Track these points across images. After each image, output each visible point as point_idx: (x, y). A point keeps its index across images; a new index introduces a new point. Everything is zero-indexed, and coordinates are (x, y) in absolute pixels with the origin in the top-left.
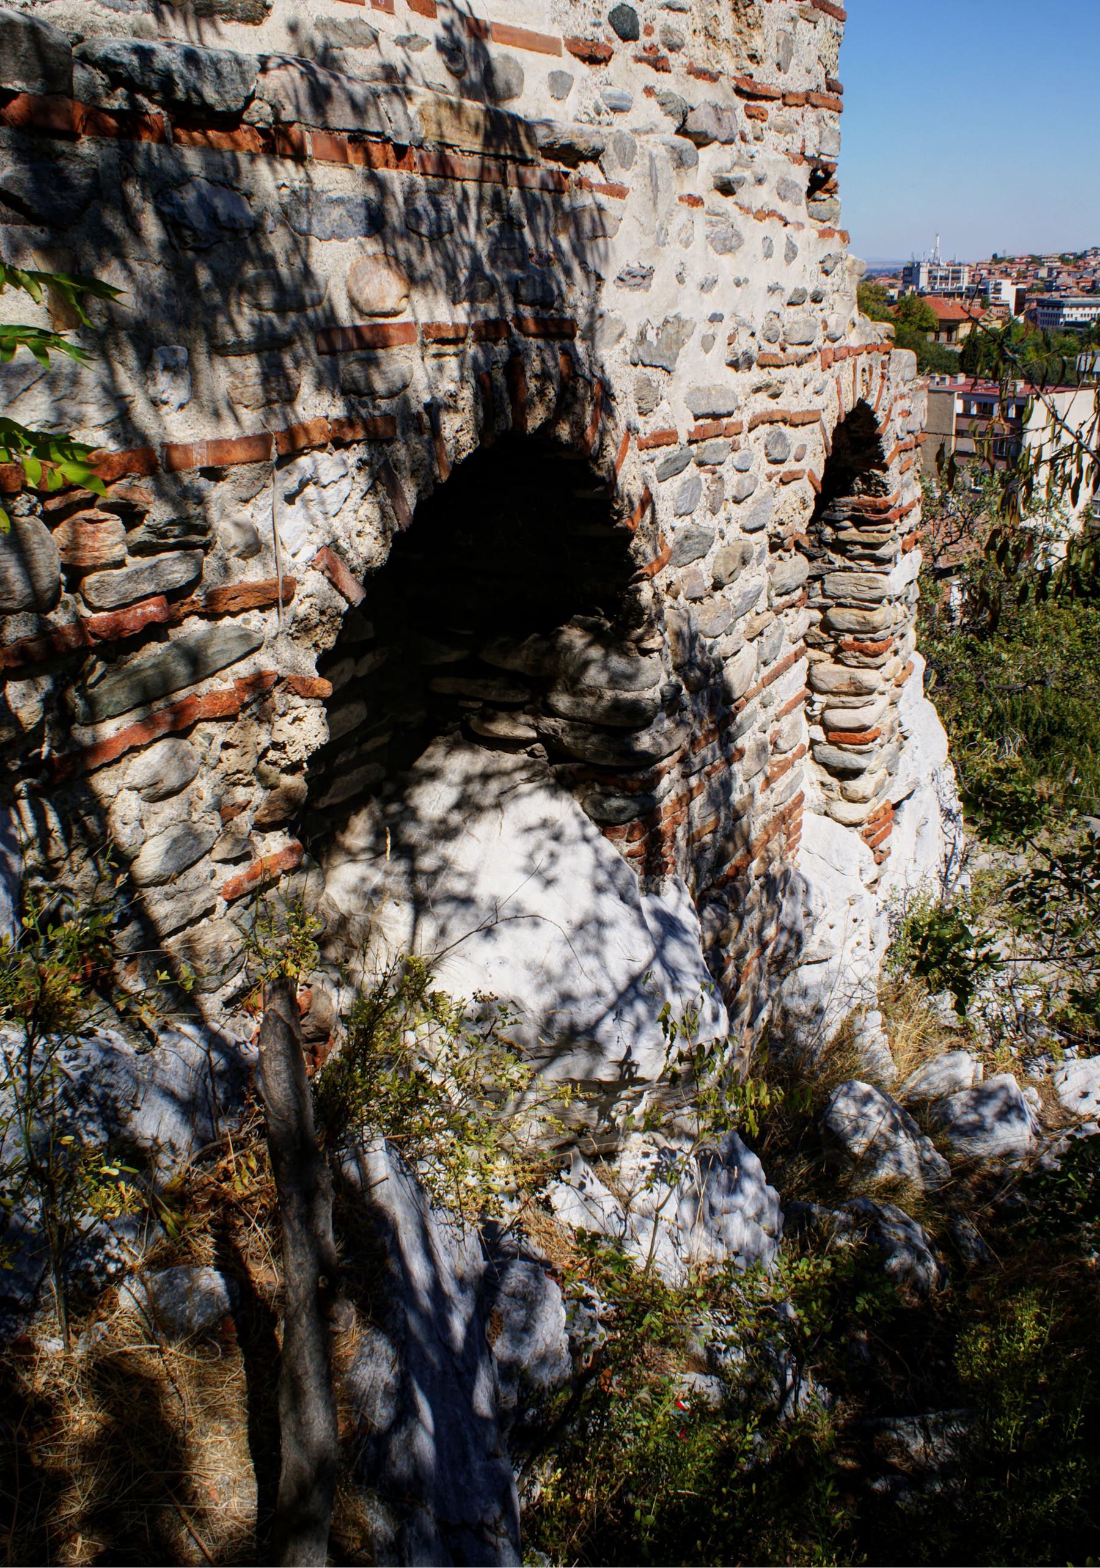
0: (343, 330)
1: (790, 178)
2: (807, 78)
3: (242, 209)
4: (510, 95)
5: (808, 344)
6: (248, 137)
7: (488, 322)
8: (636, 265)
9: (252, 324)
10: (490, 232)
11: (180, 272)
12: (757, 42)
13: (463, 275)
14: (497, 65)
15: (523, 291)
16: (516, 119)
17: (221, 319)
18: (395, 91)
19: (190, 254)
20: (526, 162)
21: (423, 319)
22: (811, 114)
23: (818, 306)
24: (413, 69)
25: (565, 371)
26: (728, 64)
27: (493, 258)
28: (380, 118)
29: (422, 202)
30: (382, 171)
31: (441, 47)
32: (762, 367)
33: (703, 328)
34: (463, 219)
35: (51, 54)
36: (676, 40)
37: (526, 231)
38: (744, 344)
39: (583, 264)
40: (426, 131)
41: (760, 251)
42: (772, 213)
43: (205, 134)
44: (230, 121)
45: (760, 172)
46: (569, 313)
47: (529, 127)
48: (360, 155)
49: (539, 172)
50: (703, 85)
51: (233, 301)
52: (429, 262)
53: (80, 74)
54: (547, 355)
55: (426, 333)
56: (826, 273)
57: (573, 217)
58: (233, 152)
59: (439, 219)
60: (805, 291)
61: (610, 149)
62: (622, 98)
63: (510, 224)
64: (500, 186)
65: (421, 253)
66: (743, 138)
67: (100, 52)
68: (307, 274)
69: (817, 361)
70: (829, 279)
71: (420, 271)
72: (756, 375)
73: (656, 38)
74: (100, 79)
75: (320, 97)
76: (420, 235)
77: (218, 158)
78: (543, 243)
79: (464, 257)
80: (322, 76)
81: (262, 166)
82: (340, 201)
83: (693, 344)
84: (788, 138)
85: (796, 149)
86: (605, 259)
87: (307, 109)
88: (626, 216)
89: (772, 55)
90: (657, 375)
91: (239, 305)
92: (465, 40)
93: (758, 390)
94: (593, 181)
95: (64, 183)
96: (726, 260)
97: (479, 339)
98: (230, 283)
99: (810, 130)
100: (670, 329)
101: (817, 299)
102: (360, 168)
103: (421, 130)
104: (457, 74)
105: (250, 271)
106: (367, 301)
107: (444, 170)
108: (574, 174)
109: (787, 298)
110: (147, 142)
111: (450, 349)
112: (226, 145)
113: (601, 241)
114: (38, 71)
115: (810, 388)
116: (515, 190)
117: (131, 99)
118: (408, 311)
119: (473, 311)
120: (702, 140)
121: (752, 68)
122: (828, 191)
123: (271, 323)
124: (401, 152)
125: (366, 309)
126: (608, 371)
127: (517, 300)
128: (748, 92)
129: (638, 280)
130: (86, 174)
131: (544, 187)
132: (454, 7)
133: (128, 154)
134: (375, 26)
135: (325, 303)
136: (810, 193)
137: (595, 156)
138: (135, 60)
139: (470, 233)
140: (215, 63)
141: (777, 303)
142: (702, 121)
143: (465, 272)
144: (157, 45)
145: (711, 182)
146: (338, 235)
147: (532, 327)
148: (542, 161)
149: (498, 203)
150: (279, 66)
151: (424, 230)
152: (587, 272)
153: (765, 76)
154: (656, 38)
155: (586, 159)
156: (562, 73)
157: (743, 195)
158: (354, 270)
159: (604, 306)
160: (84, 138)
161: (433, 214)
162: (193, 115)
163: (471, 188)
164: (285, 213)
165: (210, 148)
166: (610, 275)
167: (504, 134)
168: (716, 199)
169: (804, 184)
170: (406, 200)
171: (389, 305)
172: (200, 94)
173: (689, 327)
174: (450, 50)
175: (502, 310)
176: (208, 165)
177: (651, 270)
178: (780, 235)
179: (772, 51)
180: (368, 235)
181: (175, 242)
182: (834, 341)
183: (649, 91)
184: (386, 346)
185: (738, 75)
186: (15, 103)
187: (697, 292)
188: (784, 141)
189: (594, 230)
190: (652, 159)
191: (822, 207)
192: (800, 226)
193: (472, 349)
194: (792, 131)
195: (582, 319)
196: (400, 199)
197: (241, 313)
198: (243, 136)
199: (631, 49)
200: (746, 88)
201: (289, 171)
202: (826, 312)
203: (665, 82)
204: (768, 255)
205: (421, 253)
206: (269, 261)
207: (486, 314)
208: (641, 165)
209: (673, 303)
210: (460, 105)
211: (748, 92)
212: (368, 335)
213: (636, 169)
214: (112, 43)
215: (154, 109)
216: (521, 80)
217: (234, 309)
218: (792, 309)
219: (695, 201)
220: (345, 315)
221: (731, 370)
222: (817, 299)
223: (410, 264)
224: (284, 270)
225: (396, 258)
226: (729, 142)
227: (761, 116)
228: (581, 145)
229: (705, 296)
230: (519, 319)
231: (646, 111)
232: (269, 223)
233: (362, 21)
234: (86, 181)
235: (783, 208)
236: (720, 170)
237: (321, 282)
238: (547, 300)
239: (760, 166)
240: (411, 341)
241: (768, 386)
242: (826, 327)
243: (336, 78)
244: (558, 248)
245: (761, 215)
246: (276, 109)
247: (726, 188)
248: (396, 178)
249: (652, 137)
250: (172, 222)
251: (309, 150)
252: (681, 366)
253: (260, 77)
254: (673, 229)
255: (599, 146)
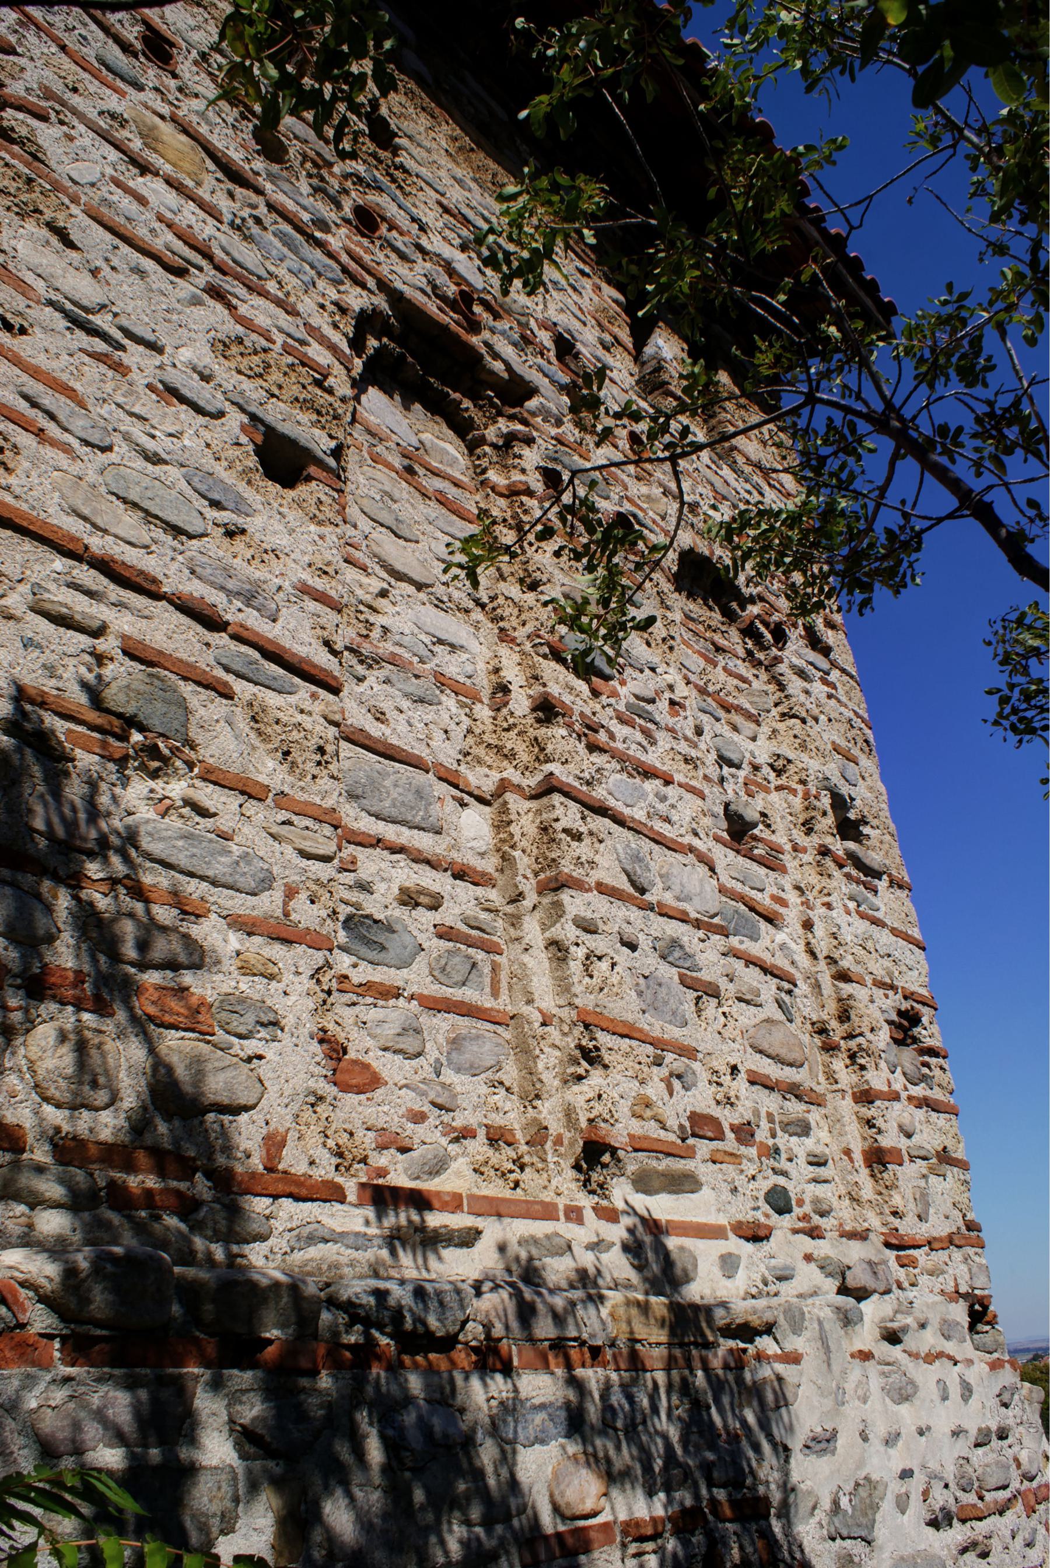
0: (546, 1538)
1: (950, 1317)
2: (947, 1222)
3: (456, 1425)
4: (688, 1279)
5: (1005, 1487)
6: (463, 1355)
7: (684, 1512)
8: (819, 1429)
9: (461, 1542)
10: (679, 1418)
11: (396, 1489)
12: (897, 1200)
13: (658, 1464)
14: (675, 1255)
15: (715, 1475)
16: (695, 1308)
17: (433, 1539)
18: (590, 1297)
19: (408, 1474)
20: (708, 1345)
21: (622, 1516)
22: (957, 1255)
23: (1006, 1443)
24: (603, 1270)
25: (765, 1557)
26: (874, 1221)
27: (685, 1440)
28: (577, 1325)
29: (617, 1398)
30: (579, 1372)
31: (626, 1248)
32: (964, 1521)
33: (896, 1487)
34: (655, 1410)
35: (305, 1305)
36: (825, 1207)
37: (713, 1410)
38: (940, 1498)
39: (770, 1436)
40: (618, 1331)
41: (935, 1393)
42: (940, 1355)
43: (426, 1357)
44: (447, 1343)
45: (922, 1317)
46: (761, 1489)
47: (708, 1310)
48: (561, 1359)
49: (721, 1352)
50: (855, 1245)
51: (444, 1519)
52: (625, 1457)
53: (326, 1316)
54: (746, 1543)
55: (625, 1533)
56: (1006, 1405)
57: (756, 1391)
58: (450, 1372)
59: (633, 1410)
60: (988, 1429)
61: (781, 1320)
62: (786, 1268)
63: (697, 1406)
64: (687, 1372)
65: (618, 1448)
66: (900, 1287)
67: (345, 1295)
68: (513, 1484)
69: (1019, 1506)
70: (1010, 1412)
71: (618, 1465)
72: (958, 1534)
73: (807, 1208)
74: (342, 1318)
75: (526, 1312)
76: (616, 1429)
77: (436, 1379)
78: (730, 1420)
79: (658, 1447)
80: (528, 1294)
81: (475, 1383)
82: (542, 1407)
83: (887, 1506)
84: (941, 1279)
85: (950, 1288)
86: (790, 1429)
87: (514, 1324)
88: (804, 1379)
89: (911, 1210)
90: (856, 1548)
91: (450, 1523)
92: (648, 1239)
93: (964, 1550)
94: (770, 1352)
95: (301, 1415)
96: (904, 1409)
97: (677, 1532)
98: (445, 1503)
99: (958, 1268)
100: (863, 1493)
101: (1002, 1435)
102: (560, 1372)
103: (612, 1330)
104: (639, 1268)
105: (462, 1487)
106: (568, 1504)
107: (636, 1363)
108: (751, 1349)
109: (972, 1440)
110: (377, 1371)
111: (650, 1546)
112: (444, 1365)
113: (783, 1410)
114: (293, 1319)
115: (1019, 1540)
116: (700, 1373)
117: (367, 1334)
118: (608, 1509)
119: (670, 1501)
120: (861, 1294)
121: (896, 1222)
122: (988, 1323)
123: (478, 1539)
124: (596, 1352)
125: (568, 1513)
126: (807, 1550)
127: (710, 1485)
128: (897, 1244)
129: (824, 1445)
130: (321, 1406)
131: (726, 1367)
132: (636, 1213)
133: (360, 1382)
134: (568, 1236)
135: (529, 1511)
136: (972, 1328)
137: (768, 1329)
138: (372, 1300)
139: (662, 1423)
140: (438, 1293)
141: (963, 1447)
142: (858, 1277)
143: (659, 1462)
144: (392, 1286)
145: (877, 1333)
146: (541, 1440)
147: (728, 1512)
148: (721, 1340)
149: (686, 1388)
150: (492, 1290)
151: (619, 1424)
152: (774, 1444)
153: (909, 1227)
154: (807, 1208)
155: (760, 1334)
156: (730, 1254)
157: (910, 1341)
158: (556, 1474)
159: (795, 1477)
160: (324, 1372)
161: (627, 1407)
162: (418, 1341)
163: (660, 1377)
164: (493, 1423)
165: (430, 1371)
166: (796, 1444)
167: (689, 1324)
168: (884, 1350)
169: (964, 1320)
170: (602, 1397)
171: (589, 1506)
172: (424, 1324)
173: (880, 1488)
174: (633, 1249)
175: (697, 1497)
176: (427, 1387)
177: (835, 1433)
178: (952, 1375)
179: (912, 1205)
180: (568, 1436)
181: (394, 1464)
182: (1031, 1479)
183: (808, 1258)
184: (587, 1551)
185: (884, 1230)
186: (270, 1349)
187: (882, 1448)
188: (937, 1283)
189: (777, 1400)
190: (820, 1323)
191: (987, 1339)
192: (970, 1362)
193: (671, 1544)
194: (943, 1272)
195: (776, 1497)
196: (596, 1396)
197: (451, 1531)
198: (460, 1356)
199: (786, 1221)
200: (894, 1241)
201: (499, 1385)
202: (1016, 1448)
203: (822, 1248)
204: (945, 1398)
205: (618, 1448)
206: (478, 1474)
207: (682, 1503)
208: (811, 1329)
209: (861, 1464)
210: (647, 1302)
211: (897, 1244)
212: (570, 1541)
213: (807, 1334)
214: (356, 1288)
215: (384, 1341)
216: (696, 1266)
217: (445, 1527)
218: (980, 1451)
219: (865, 1356)
220: (548, 1522)
221: (930, 1530)
222: (1002, 1435)
223: (608, 1461)
224: (492, 1482)
225: (595, 1455)
226: (888, 1292)
227: (913, 1263)
228: (755, 1321)
229: (892, 1451)
230: (713, 1502)
231: (809, 1276)
232: (480, 1435)
233: (557, 1234)
234: (321, 1412)
235: (950, 1347)
236: (883, 1320)
237: (526, 1490)
238: (737, 1477)
239: (920, 1310)
240: (610, 1542)
241: (974, 1544)
242: (1019, 1465)
243: (540, 1294)
244: (744, 1423)
245: (931, 1358)
246: (488, 1327)
247: (893, 1337)
248: (592, 1376)
249: (817, 1300)
250: (390, 1445)
251: (516, 1362)
252: (881, 1533)
253: (474, 1301)
254: (849, 1386)
255: (771, 1320)
